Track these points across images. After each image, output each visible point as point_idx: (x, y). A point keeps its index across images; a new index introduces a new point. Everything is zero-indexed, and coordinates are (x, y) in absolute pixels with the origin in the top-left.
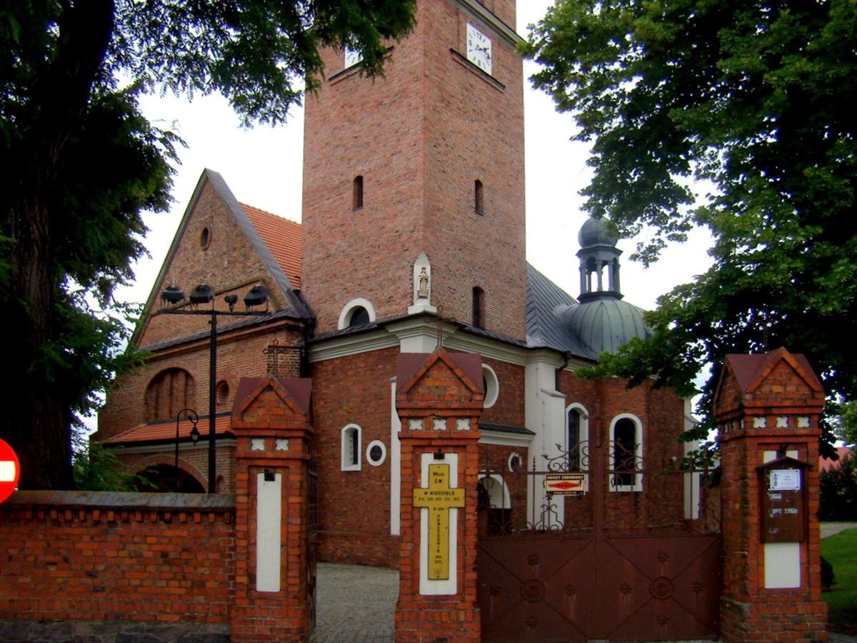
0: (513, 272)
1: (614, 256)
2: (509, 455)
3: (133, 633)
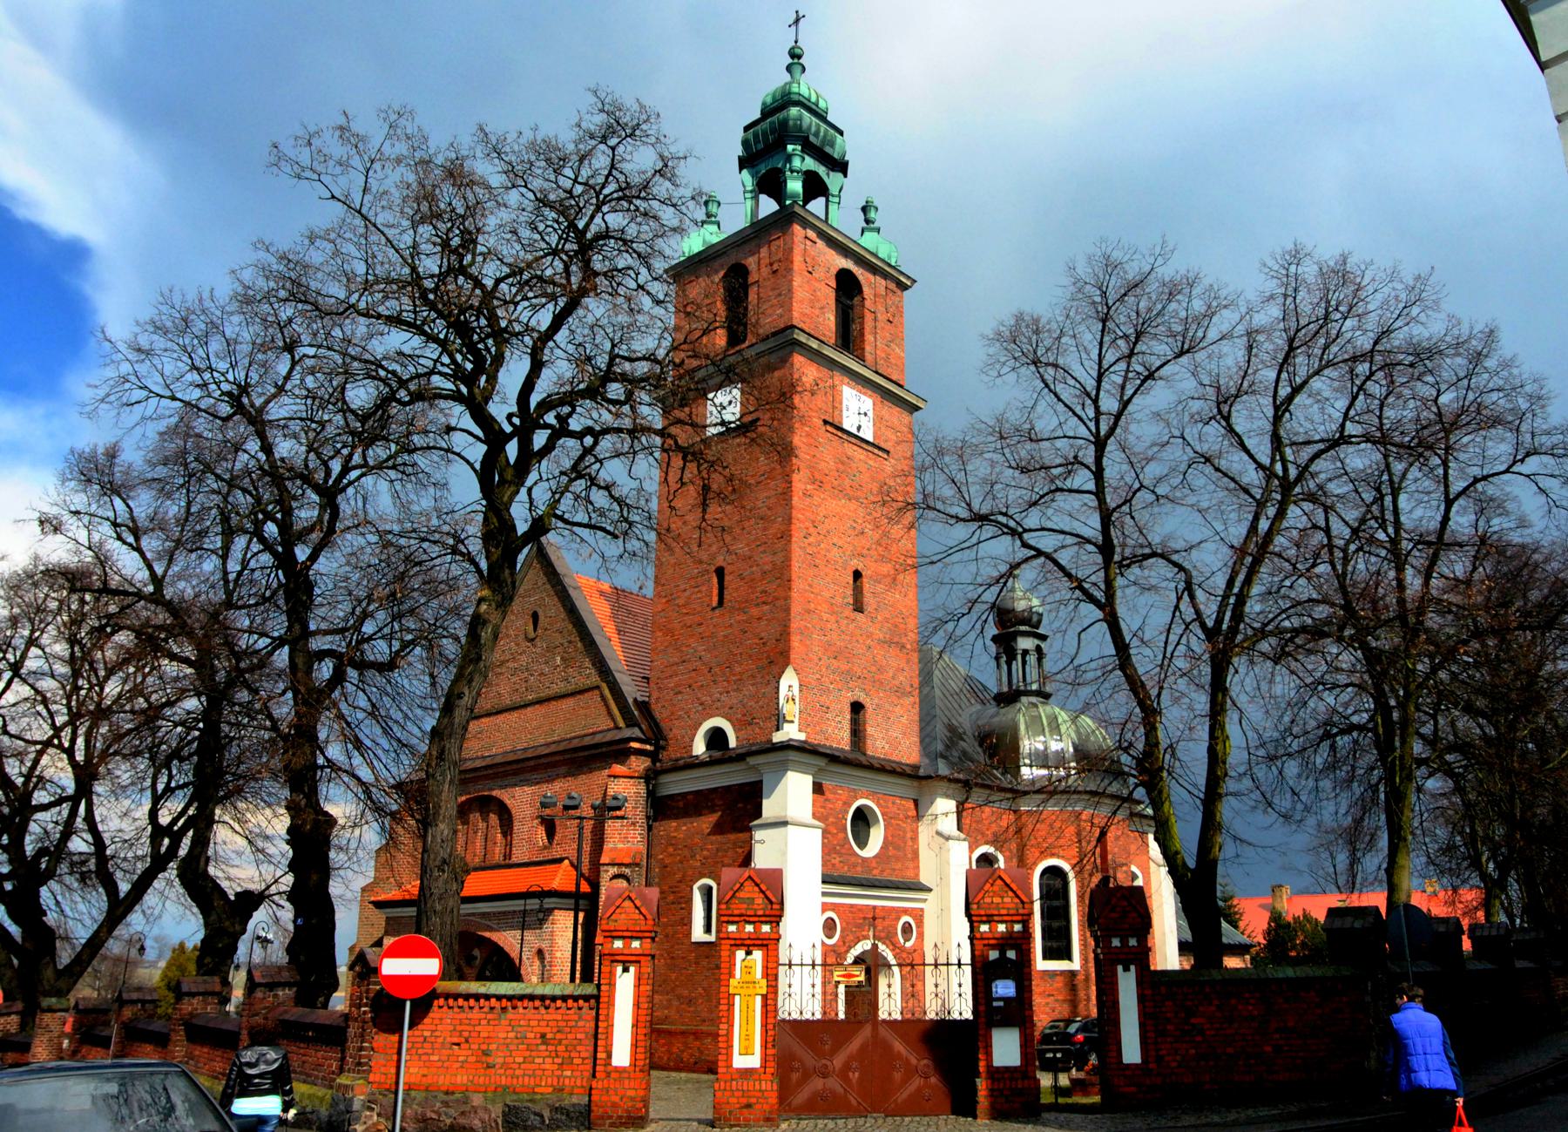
2: (898, 919)
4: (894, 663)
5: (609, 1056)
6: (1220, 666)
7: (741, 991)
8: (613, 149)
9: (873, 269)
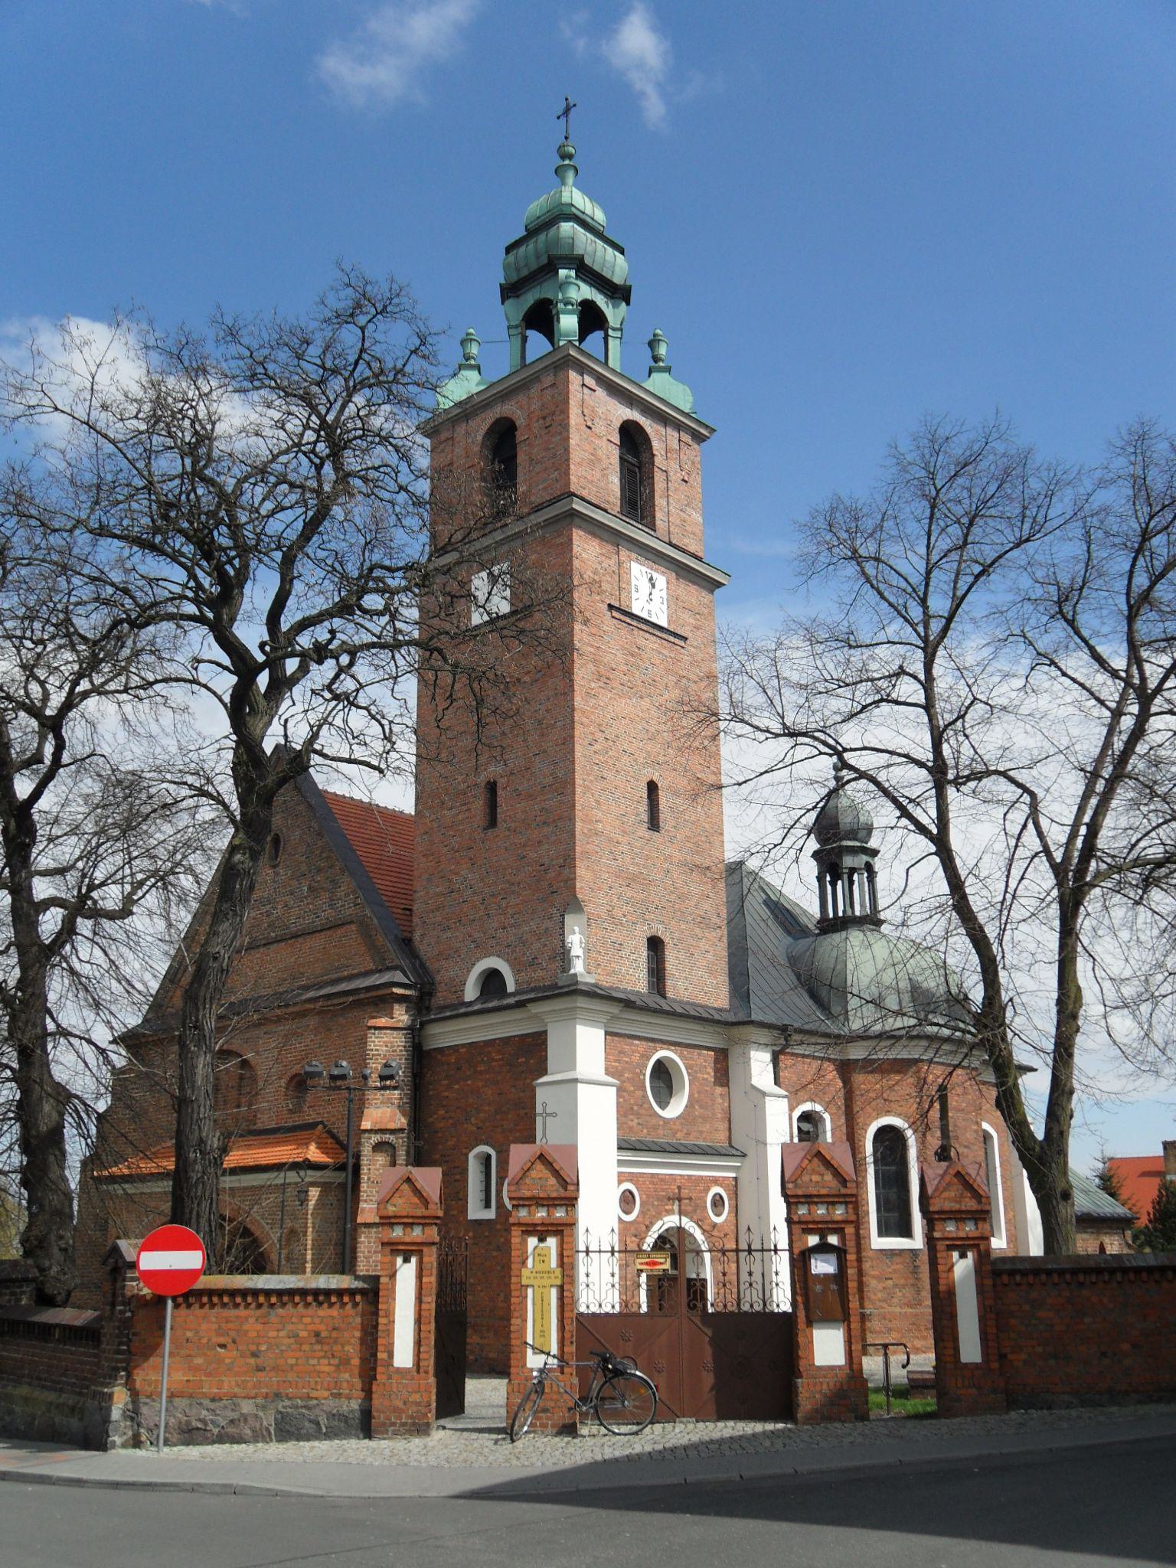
0: (706, 907)
1: (865, 858)
2: (707, 1190)
3: (289, 1410)
4: (695, 889)
5: (391, 1355)
6: (1070, 905)
7: (535, 1283)
8: (363, 329)
9: (663, 419)
